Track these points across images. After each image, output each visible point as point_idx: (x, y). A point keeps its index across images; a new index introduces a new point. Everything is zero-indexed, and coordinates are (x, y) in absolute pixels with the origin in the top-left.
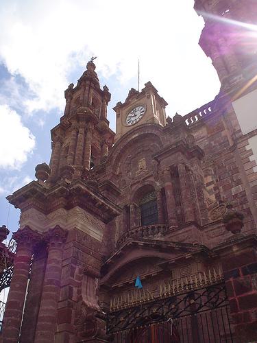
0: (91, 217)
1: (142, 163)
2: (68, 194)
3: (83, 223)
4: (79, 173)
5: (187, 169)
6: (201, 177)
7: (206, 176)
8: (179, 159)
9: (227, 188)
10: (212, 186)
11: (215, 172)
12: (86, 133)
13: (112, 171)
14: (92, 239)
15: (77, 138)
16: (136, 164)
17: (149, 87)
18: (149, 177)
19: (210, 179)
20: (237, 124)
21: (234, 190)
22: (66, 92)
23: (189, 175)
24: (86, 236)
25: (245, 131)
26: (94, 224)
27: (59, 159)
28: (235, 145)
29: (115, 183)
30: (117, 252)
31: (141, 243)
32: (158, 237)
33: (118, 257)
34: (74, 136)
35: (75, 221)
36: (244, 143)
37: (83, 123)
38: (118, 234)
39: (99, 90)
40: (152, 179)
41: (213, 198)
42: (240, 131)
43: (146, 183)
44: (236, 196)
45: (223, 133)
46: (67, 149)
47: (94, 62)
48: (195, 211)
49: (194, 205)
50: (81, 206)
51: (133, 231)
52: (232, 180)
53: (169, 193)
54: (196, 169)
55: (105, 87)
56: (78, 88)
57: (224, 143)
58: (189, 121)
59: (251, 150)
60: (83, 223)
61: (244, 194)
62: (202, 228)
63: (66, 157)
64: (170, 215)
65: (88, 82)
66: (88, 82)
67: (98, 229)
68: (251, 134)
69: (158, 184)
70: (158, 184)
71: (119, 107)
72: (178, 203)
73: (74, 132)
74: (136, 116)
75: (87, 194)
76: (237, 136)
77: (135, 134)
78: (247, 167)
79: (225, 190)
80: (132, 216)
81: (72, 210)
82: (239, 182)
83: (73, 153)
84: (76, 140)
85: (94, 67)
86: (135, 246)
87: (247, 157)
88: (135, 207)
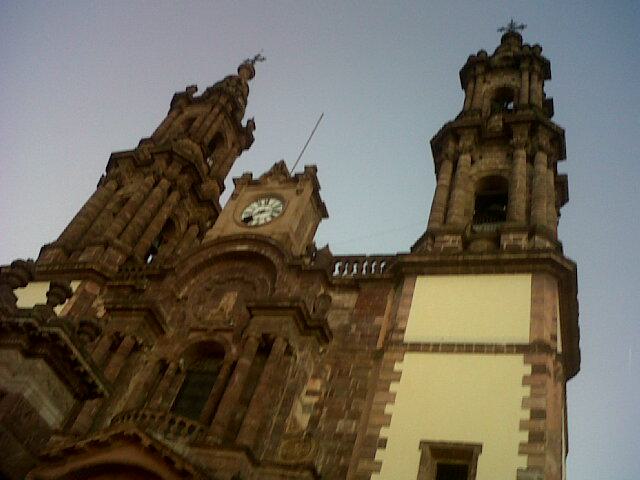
0: (57, 383)
1: (229, 300)
2: (37, 334)
3: (37, 389)
4: (120, 258)
5: (289, 351)
6: (306, 376)
7: (315, 377)
8: (284, 327)
9: (335, 415)
10: (314, 400)
11: (332, 377)
12: (170, 191)
13: (172, 286)
14: (39, 420)
15: (151, 191)
16: (218, 296)
17: (311, 173)
18: (227, 331)
19: (317, 385)
20: (405, 318)
21: (341, 425)
22: (177, 97)
23: (287, 364)
24: (32, 412)
25: (409, 336)
26: (55, 398)
27: (99, 213)
28: (382, 351)
29: (167, 313)
30: (100, 437)
31: (146, 442)
32: (179, 446)
33: (97, 445)
34: (146, 185)
35: (27, 383)
36: (396, 355)
37: (174, 170)
38: (124, 404)
39: (236, 122)
40: (228, 336)
41: (304, 420)
42: (403, 331)
43: (217, 338)
44: (339, 436)
45: (378, 320)
46: (124, 201)
47: (258, 66)
48: (261, 431)
49: (268, 417)
50: (49, 362)
51: (148, 413)
52: (349, 407)
53: (238, 377)
54: (305, 357)
55: (252, 124)
56: (200, 100)
57: (370, 336)
58: (342, 270)
59: (400, 373)
60: (37, 389)
61: (352, 439)
62: (256, 463)
63: (114, 215)
64: (219, 415)
65: (223, 100)
66: (223, 100)
67: (59, 406)
68: (416, 347)
69: (234, 350)
70: (234, 350)
71: (246, 181)
72: (245, 402)
73: (150, 180)
74: (262, 213)
75: (66, 351)
76: (394, 337)
77: (242, 244)
78: (379, 397)
79: (329, 416)
80: (165, 383)
81: (30, 362)
82: (355, 416)
83: (129, 216)
84: (146, 197)
85: (252, 75)
86: (135, 440)
87: (388, 383)
88: (178, 371)
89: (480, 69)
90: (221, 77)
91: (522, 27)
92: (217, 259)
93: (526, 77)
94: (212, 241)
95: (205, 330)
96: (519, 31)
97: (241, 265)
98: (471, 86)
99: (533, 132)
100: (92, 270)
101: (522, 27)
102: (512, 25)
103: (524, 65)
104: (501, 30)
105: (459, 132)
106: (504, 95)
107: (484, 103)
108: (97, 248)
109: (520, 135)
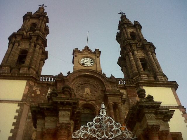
58: (42, 79)
77: (87, 72)
89: (28, 17)
90: (118, 25)
91: (46, 6)
92: (79, 76)
93: (41, 22)
94: (76, 71)
95: (86, 100)
96: (44, 7)
97: (87, 79)
98: (25, 22)
99: (131, 46)
100: (32, 77)
101: (46, 6)
102: (43, 5)
103: (41, 18)
104: (40, 6)
105: (132, 44)
106: (34, 25)
107: (28, 27)
108: (26, 68)
109: (34, 39)
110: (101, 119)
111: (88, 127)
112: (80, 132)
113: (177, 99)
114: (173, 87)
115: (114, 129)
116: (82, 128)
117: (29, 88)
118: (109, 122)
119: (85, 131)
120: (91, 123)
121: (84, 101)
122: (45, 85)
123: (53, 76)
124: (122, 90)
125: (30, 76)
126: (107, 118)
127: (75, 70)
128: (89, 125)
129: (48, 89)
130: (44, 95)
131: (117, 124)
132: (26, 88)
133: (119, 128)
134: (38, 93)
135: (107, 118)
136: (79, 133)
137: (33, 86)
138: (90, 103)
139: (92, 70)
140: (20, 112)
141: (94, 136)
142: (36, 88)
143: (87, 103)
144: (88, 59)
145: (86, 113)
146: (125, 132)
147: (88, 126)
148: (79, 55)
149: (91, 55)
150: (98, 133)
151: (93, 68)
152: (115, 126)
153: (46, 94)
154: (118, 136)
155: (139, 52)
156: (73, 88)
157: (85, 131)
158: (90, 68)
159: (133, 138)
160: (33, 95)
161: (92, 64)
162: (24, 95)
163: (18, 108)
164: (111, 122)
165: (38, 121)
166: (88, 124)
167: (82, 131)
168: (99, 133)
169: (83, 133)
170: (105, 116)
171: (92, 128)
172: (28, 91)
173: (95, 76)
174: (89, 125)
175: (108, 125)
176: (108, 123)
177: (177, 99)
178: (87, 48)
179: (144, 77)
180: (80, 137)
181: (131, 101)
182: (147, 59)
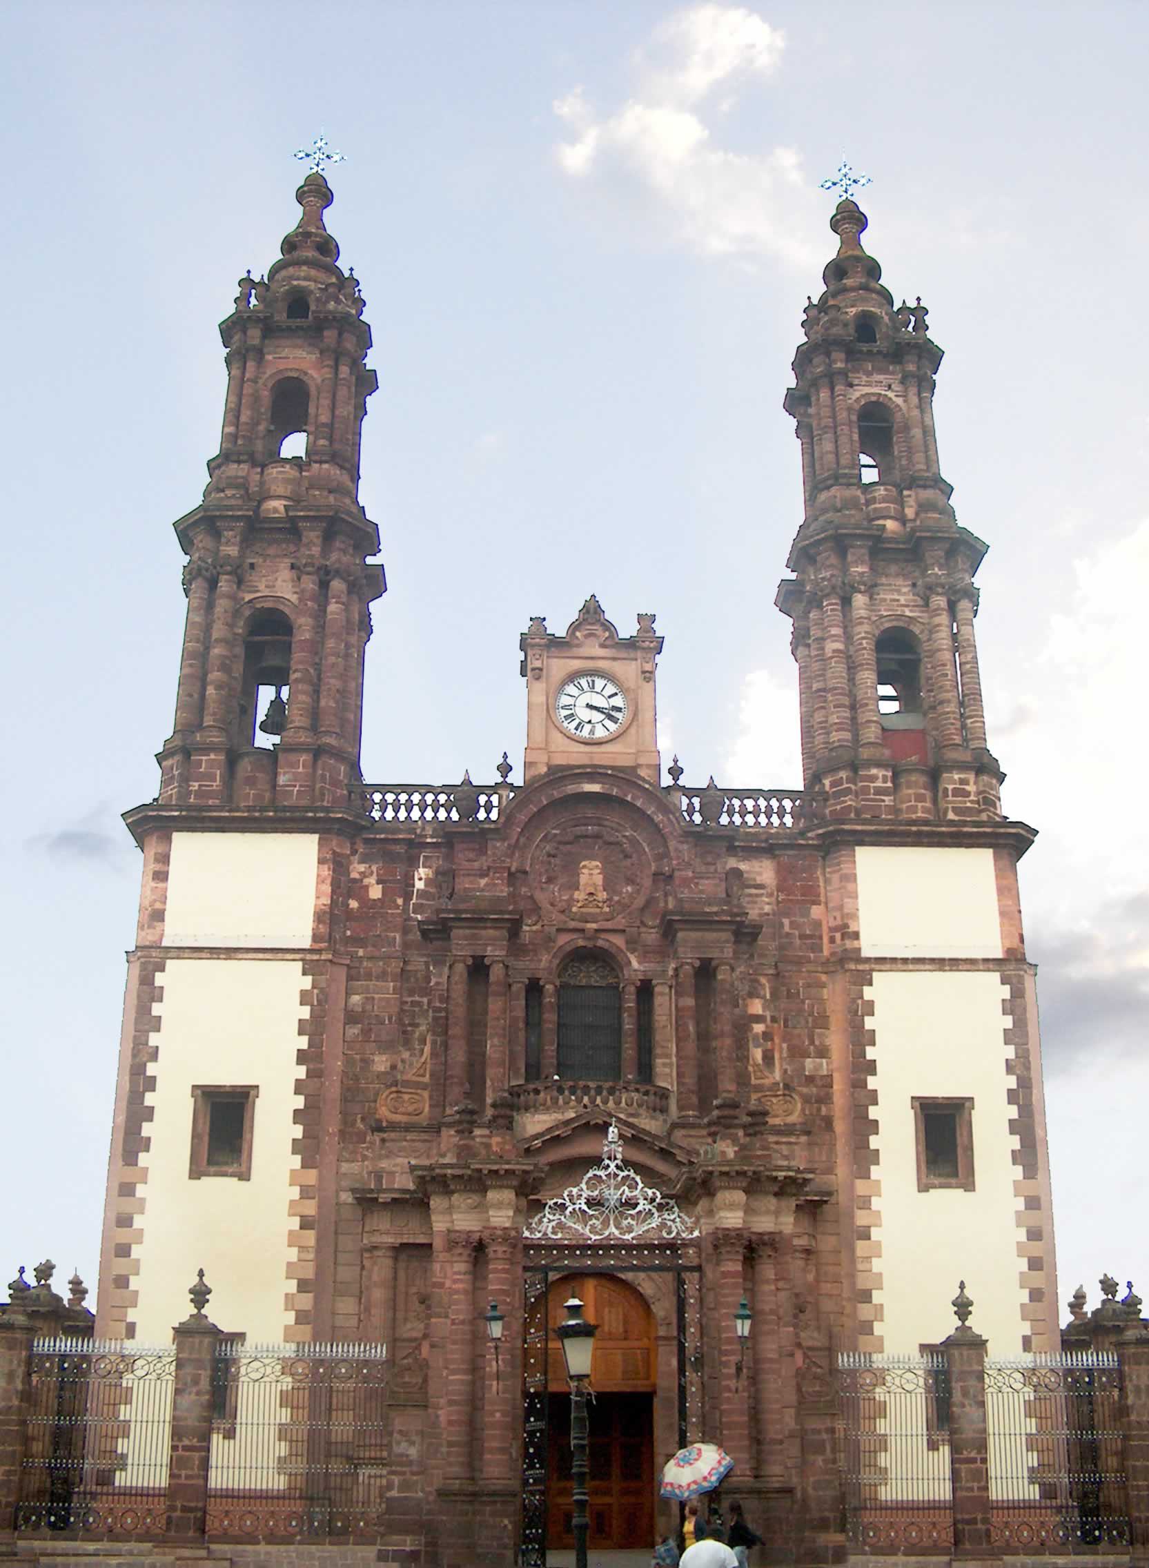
108: (303, 758)
110: (604, 1178)
111: (568, 1203)
112: (545, 1220)
113: (1011, 913)
114: (1005, 846)
115: (639, 1208)
116: (550, 1207)
117: (336, 864)
118: (625, 1187)
119: (557, 1216)
120: (575, 1191)
121: (575, 936)
122: (400, 849)
123: (428, 789)
124: (756, 858)
125: (332, 815)
126: (622, 1174)
127: (533, 772)
128: (570, 1196)
129: (413, 863)
130: (400, 901)
131: (650, 1192)
132: (320, 880)
133: (655, 1204)
134: (376, 892)
135: (622, 1174)
136: (540, 1221)
137: (348, 856)
138: (600, 943)
139: (612, 768)
140: (315, 1003)
141: (582, 1231)
142: (362, 868)
143: (589, 944)
144: (600, 683)
145: (584, 982)
146: (668, 1217)
147: (567, 1199)
148: (559, 666)
149: (614, 659)
150: (594, 1221)
151: (617, 755)
152: (641, 1201)
153: (407, 897)
154: (648, 1231)
155: (891, 581)
156: (528, 869)
157: (557, 1216)
158: (604, 748)
159: (690, 1236)
160: (354, 904)
161: (615, 720)
162: (319, 917)
163: (307, 982)
164: (633, 1187)
165: (432, 1202)
166: (566, 1193)
167: (551, 1217)
168: (597, 1223)
169: (554, 1223)
170: (617, 1167)
171: (577, 1207)
172: (333, 892)
173: (629, 798)
174: (570, 1196)
175: (624, 1197)
176: (624, 1191)
177: (1011, 913)
178: (592, 612)
179: (873, 779)
180: (545, 1234)
181: (787, 929)
182: (923, 637)
